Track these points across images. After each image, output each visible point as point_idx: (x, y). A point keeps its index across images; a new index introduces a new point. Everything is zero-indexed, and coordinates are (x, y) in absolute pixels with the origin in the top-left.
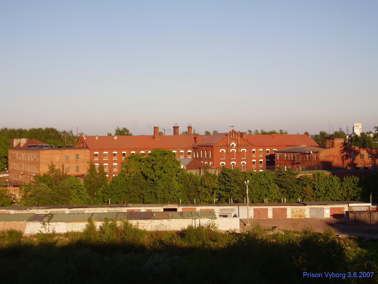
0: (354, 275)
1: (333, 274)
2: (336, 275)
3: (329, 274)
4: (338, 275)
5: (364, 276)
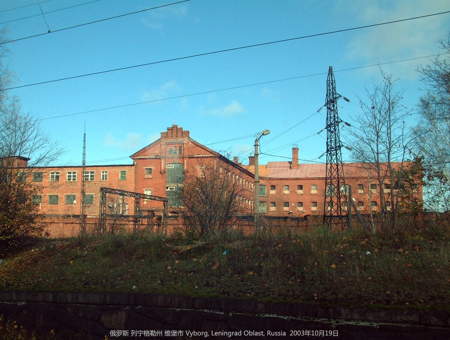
0: (332, 333)
1: (194, 333)
2: (197, 334)
3: (190, 333)
4: (199, 334)
5: (295, 334)
